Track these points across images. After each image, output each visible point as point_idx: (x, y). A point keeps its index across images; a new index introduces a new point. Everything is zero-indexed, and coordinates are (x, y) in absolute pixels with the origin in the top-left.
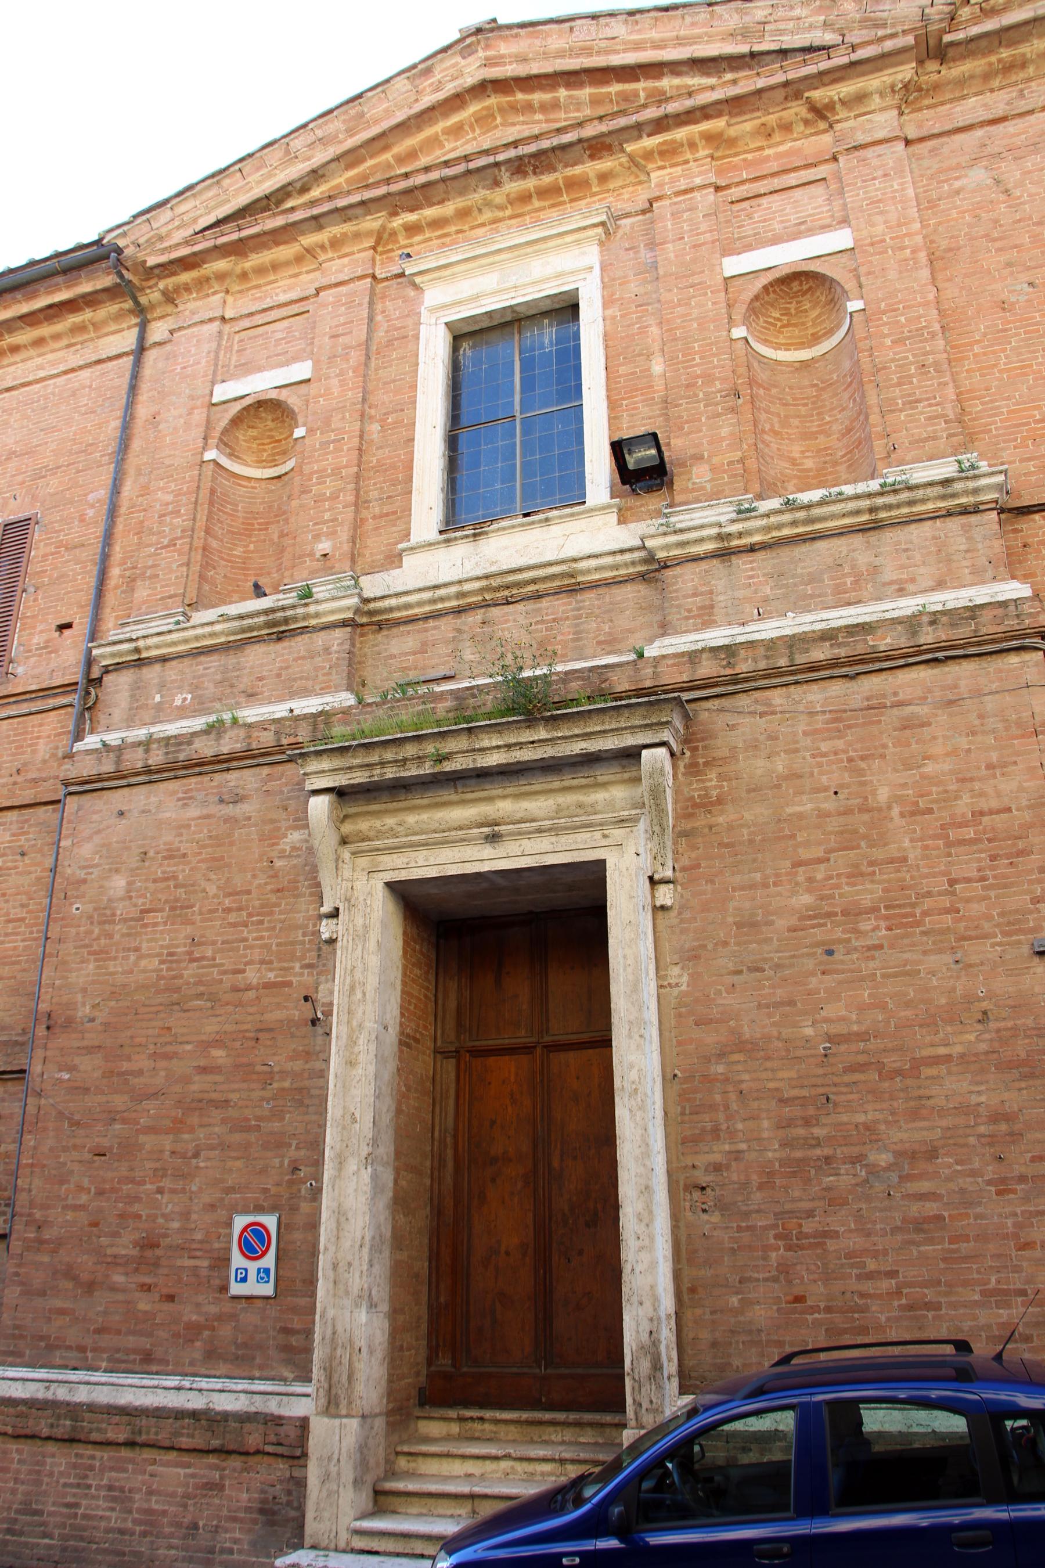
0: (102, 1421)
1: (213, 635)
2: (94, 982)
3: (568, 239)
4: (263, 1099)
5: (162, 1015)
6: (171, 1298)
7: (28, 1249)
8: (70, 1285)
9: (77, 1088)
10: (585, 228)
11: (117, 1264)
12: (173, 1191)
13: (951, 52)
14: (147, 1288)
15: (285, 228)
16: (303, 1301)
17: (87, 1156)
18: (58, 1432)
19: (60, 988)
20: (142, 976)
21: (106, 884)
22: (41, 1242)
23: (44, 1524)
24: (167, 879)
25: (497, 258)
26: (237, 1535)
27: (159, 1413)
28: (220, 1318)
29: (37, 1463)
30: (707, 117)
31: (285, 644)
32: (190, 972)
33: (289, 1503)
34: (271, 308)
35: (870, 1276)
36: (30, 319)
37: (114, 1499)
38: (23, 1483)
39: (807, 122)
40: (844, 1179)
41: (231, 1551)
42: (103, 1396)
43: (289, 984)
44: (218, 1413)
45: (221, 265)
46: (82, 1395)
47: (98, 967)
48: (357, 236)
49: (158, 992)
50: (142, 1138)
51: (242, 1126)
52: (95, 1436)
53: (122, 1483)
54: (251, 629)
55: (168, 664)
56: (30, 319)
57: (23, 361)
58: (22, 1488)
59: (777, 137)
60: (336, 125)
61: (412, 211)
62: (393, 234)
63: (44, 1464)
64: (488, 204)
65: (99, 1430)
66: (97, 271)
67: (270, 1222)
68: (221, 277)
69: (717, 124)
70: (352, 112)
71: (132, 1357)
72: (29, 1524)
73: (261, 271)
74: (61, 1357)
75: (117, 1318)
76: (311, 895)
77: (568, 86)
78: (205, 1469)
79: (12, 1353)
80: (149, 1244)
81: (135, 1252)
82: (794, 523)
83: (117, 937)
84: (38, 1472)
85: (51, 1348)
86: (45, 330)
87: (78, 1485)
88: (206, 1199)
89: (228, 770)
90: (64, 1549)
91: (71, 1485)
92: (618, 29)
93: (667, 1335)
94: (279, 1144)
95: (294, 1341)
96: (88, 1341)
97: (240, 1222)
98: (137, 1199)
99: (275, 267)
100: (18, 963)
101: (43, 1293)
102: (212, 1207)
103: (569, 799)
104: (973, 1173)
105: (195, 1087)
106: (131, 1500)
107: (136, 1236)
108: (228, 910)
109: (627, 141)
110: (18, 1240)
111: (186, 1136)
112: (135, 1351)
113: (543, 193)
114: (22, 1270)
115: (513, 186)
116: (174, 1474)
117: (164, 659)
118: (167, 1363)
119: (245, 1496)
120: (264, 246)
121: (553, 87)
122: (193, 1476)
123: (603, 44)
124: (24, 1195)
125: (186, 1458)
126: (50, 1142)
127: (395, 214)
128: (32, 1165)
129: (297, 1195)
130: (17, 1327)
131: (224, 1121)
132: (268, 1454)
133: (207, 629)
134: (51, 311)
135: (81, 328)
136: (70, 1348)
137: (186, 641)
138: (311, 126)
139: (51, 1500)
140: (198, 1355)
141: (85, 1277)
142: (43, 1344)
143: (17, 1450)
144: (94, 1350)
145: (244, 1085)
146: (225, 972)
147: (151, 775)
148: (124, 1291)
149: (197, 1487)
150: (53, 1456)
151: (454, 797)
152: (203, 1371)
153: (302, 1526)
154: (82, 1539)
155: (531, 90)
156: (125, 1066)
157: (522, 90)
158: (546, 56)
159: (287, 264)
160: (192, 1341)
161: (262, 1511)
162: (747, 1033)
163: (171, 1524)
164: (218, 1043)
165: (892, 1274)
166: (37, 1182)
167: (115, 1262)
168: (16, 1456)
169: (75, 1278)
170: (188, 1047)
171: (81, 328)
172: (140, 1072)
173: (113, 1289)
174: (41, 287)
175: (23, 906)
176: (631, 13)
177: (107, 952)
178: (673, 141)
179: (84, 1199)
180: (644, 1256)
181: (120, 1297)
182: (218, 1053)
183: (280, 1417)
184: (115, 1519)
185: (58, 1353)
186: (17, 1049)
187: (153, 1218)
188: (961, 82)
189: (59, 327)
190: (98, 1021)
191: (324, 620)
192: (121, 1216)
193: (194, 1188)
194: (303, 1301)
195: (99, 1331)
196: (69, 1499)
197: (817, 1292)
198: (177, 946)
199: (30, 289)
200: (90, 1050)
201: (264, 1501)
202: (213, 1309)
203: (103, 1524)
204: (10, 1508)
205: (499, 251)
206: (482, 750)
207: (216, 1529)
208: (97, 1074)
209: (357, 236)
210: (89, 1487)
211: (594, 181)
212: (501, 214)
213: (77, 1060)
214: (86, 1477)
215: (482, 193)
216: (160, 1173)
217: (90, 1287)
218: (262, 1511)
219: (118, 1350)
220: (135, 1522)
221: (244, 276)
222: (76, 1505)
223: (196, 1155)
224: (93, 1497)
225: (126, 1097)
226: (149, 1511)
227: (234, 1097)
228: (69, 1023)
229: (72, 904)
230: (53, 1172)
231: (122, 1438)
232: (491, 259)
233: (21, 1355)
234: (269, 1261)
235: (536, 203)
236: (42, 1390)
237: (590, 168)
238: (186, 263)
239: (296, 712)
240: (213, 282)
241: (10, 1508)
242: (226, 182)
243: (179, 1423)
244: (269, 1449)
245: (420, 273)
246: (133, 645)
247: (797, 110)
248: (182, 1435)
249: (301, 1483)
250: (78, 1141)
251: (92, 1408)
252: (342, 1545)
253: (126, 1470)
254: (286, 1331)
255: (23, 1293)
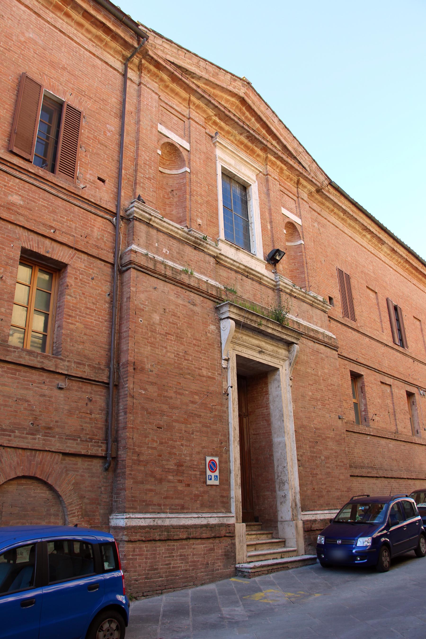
0: (178, 531)
1: (177, 233)
2: (151, 355)
3: (253, 168)
4: (210, 417)
5: (177, 377)
6: (188, 485)
7: (135, 464)
8: (153, 480)
9: (148, 398)
10: (257, 169)
11: (169, 472)
12: (186, 446)
13: (320, 193)
14: (180, 481)
15: (193, 90)
16: (226, 487)
17: (155, 428)
18: (163, 538)
19: (137, 353)
20: (168, 359)
21: (152, 315)
22: (140, 461)
23: (159, 573)
24: (174, 324)
25: (237, 157)
26: (219, 564)
27: (195, 527)
28: (204, 492)
29: (154, 551)
30: (285, 165)
31: (196, 252)
32: (185, 363)
33: (232, 551)
34: (174, 108)
35: (322, 484)
36: (86, 15)
37: (182, 559)
38: (149, 559)
39: (294, 182)
40: (318, 462)
41: (218, 570)
42: (175, 522)
43: (215, 379)
44: (212, 524)
45: (165, 77)
46: (167, 523)
47: (152, 350)
48: (205, 111)
49: (175, 368)
50: (174, 424)
51: (205, 425)
52: (176, 537)
53: (185, 553)
54: (188, 239)
55: (159, 233)
56: (86, 15)
57: (67, 23)
58: (149, 561)
59: (288, 180)
60: (211, 69)
61: (219, 119)
62: (211, 119)
63: (156, 550)
64: (235, 136)
65: (177, 535)
66: (128, 32)
67: (216, 459)
68: (162, 80)
69: (285, 168)
70: (216, 71)
71: (178, 507)
72: (154, 574)
73: (172, 91)
74: (152, 509)
75: (171, 493)
76: (218, 350)
77: (256, 120)
78: (208, 544)
79: (132, 508)
80: (180, 465)
81: (175, 468)
82: (302, 296)
83: (158, 340)
84: (155, 554)
85: (147, 505)
86: (87, 25)
87: (170, 557)
88: (197, 450)
89: (191, 291)
90: (168, 580)
91: (167, 557)
92: (276, 120)
93: (298, 497)
94: (216, 433)
95: (225, 500)
96: (162, 502)
97: (208, 459)
98: (175, 447)
99: (177, 94)
100: (94, 330)
101: (142, 483)
102: (199, 453)
103: (275, 349)
104: (334, 463)
105: (190, 408)
106: (188, 558)
107: (175, 461)
108: (195, 345)
109: (270, 154)
110: (130, 459)
111: (189, 426)
112: (178, 505)
113: (246, 146)
114: (132, 473)
115: (243, 138)
116: (200, 547)
117: (158, 230)
118: (189, 509)
119: (220, 551)
120: (181, 86)
121: (253, 116)
122: (206, 547)
123: (271, 121)
124: (131, 440)
125: (203, 541)
126: (139, 419)
127: (215, 115)
128: (133, 428)
129: (223, 451)
130: (133, 497)
131: (200, 422)
132: (227, 536)
133: (176, 230)
134: (99, 23)
135: (101, 40)
136: (155, 505)
137: (167, 229)
138: (207, 62)
139: (160, 563)
140: (198, 506)
141: (158, 476)
142: (144, 504)
143: (145, 546)
144: (164, 505)
145: (205, 411)
146: (196, 368)
147: (166, 278)
148: (173, 482)
149: (207, 550)
150: (160, 547)
151: (252, 335)
152: (200, 511)
153: (235, 558)
154: (173, 575)
155: (248, 111)
156: (166, 394)
157: (246, 108)
158: (259, 108)
159: (181, 97)
160: (196, 501)
161: (225, 555)
162: (304, 423)
163: (201, 564)
164: (196, 394)
165: (325, 484)
166: (136, 436)
167: (169, 471)
168: (145, 549)
169: (154, 477)
170: (187, 392)
171: (101, 40)
172: (171, 398)
173: (169, 481)
174: (104, 12)
175: (93, 303)
176: (281, 121)
177: (154, 345)
178: (276, 163)
179: (155, 445)
180: (292, 476)
181: (172, 485)
182: (196, 397)
183: (229, 524)
184: (183, 566)
185: (150, 507)
186: (100, 371)
187: (180, 455)
188: (316, 199)
189: (94, 30)
190: (154, 372)
191: (209, 252)
192: (170, 453)
193: (193, 446)
194: (226, 487)
195: (165, 498)
196: (167, 562)
197: (316, 487)
198: (180, 352)
199: (99, 7)
200: (153, 384)
201: (225, 552)
202: (202, 489)
203: (180, 569)
204: (145, 569)
205: (239, 156)
206: (268, 327)
207: (214, 564)
208: (156, 394)
209: (205, 111)
210: (174, 556)
211: (256, 154)
212: (234, 141)
213: (147, 387)
214: (172, 553)
215: (236, 132)
216: (182, 438)
217: (161, 481)
218: (225, 555)
219: (172, 505)
220: (190, 566)
221: (167, 87)
222: (170, 564)
223: (193, 433)
224: (175, 560)
225: (167, 406)
226: (194, 562)
227: (202, 414)
228: (143, 370)
229: (138, 318)
230: (142, 432)
231: (185, 537)
232: (235, 156)
233: (136, 508)
234: (217, 473)
235: (242, 147)
236: (152, 522)
237: (258, 151)
238: (158, 65)
239: (209, 282)
240: (158, 78)
241: (145, 569)
242: (180, 52)
243: (202, 529)
244: (227, 535)
245: (220, 143)
246: (150, 217)
247: (295, 179)
248: (203, 533)
249: (234, 544)
250: (151, 421)
251: (173, 527)
252: (245, 561)
253: (185, 548)
254: (222, 496)
255: (134, 483)
